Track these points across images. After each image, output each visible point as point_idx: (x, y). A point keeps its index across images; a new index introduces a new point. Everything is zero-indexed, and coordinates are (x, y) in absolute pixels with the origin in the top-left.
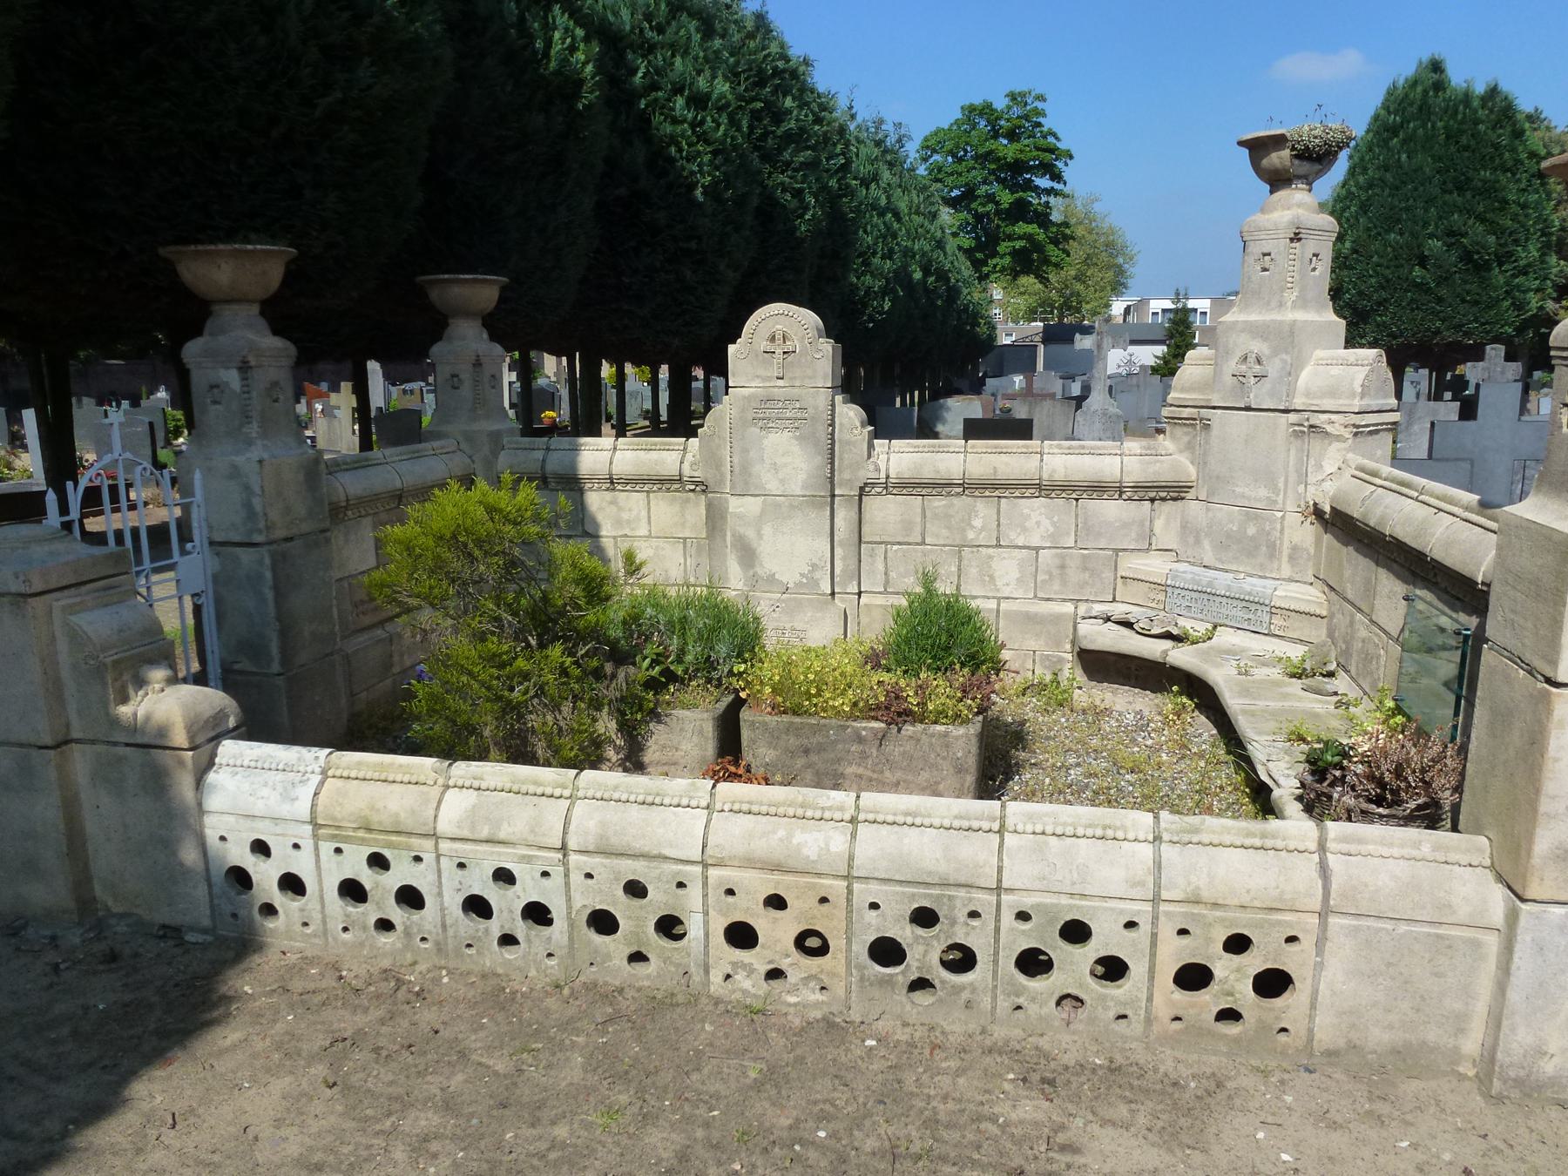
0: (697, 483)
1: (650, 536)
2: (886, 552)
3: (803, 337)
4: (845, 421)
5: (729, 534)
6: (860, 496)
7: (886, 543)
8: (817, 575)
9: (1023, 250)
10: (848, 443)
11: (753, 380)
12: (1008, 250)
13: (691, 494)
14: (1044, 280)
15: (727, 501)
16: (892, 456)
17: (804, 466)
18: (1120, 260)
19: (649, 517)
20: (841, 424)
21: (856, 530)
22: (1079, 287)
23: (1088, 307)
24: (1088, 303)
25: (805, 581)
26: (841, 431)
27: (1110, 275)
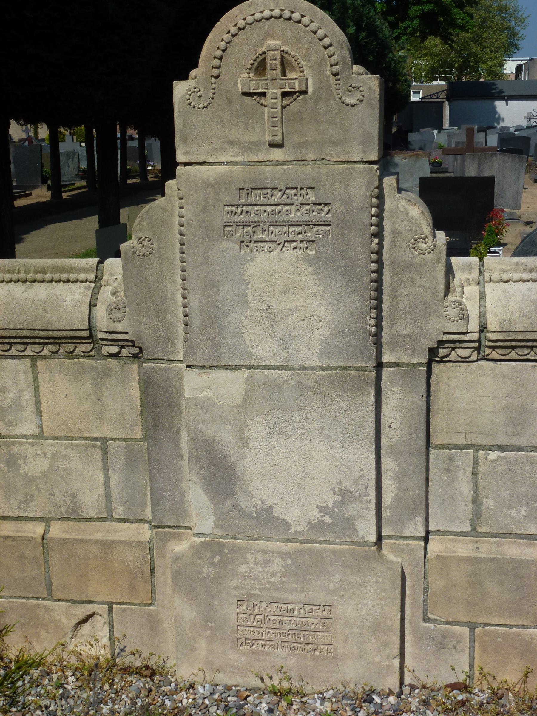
0: (122, 344)
1: (40, 436)
2: (476, 463)
3: (321, 64)
4: (403, 226)
5: (184, 434)
6: (429, 366)
7: (477, 448)
8: (352, 510)
9: (431, 12)
10: (408, 267)
11: (223, 149)
12: (418, 13)
13: (113, 362)
14: (446, 39)
15: (178, 375)
16: (489, 288)
17: (325, 313)
18: (513, 23)
19: (38, 403)
20: (395, 233)
21: (423, 427)
22: (476, 48)
23: (485, 66)
24: (484, 63)
25: (327, 519)
26: (394, 245)
27: (503, 37)
